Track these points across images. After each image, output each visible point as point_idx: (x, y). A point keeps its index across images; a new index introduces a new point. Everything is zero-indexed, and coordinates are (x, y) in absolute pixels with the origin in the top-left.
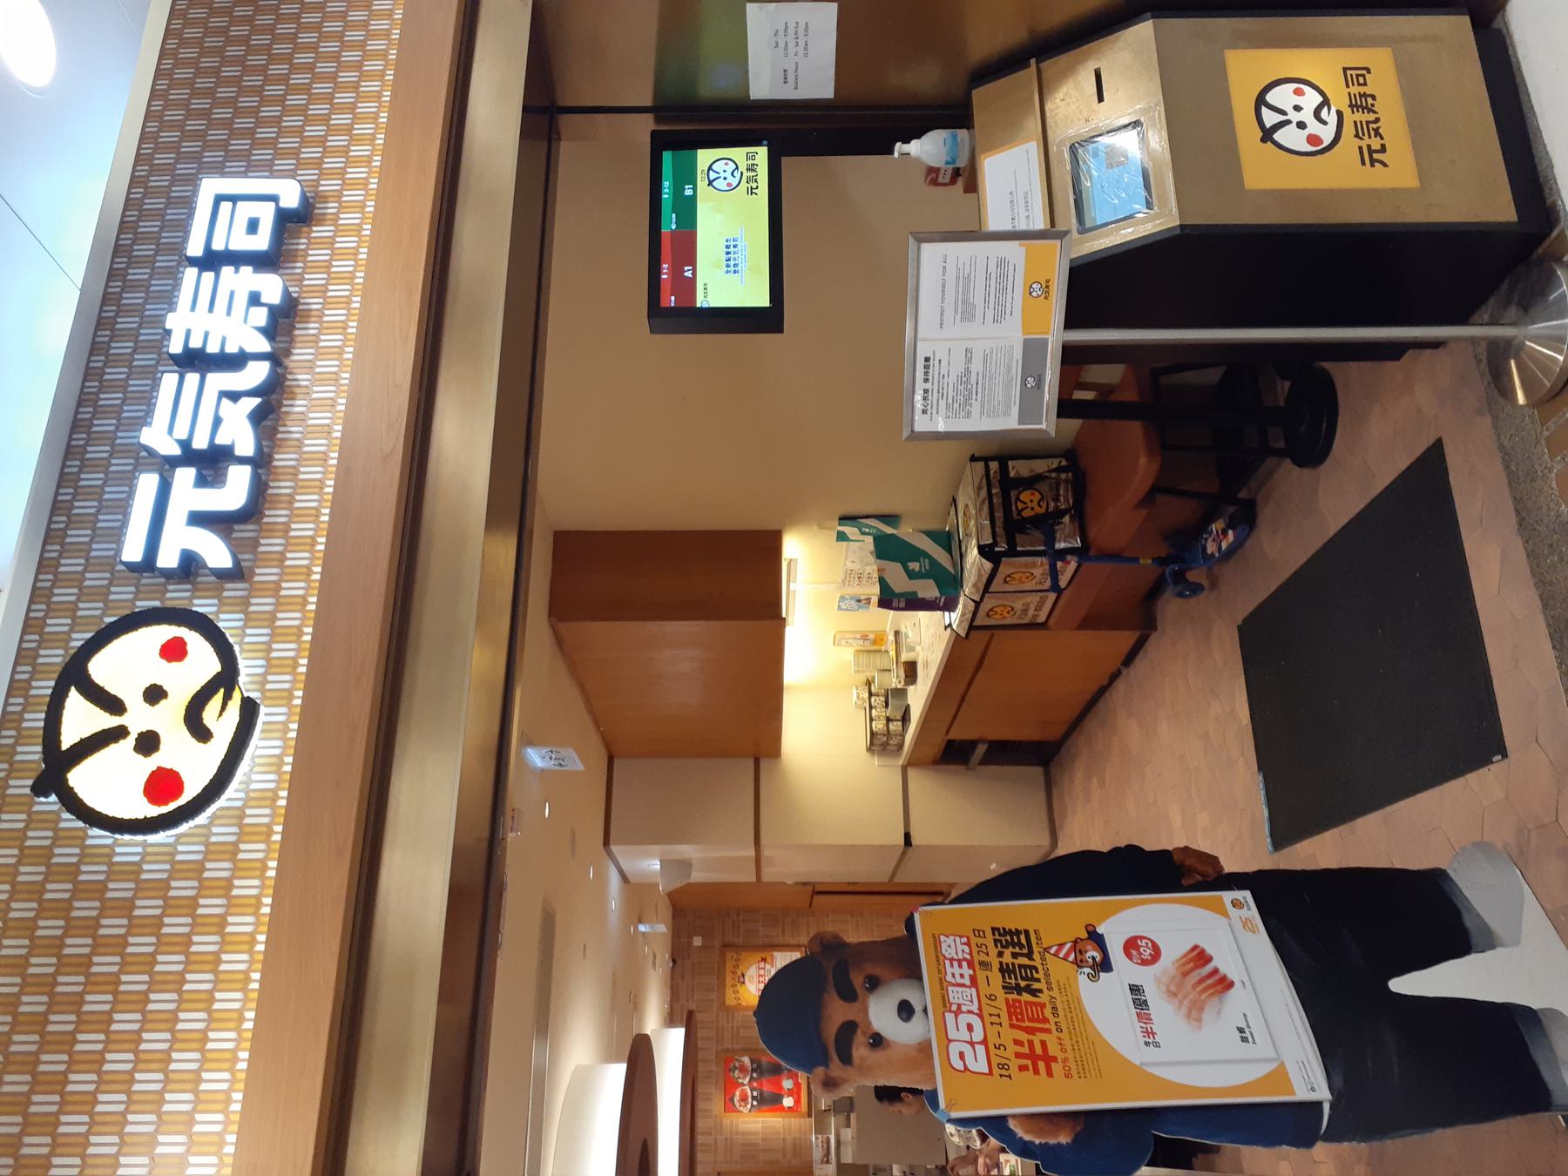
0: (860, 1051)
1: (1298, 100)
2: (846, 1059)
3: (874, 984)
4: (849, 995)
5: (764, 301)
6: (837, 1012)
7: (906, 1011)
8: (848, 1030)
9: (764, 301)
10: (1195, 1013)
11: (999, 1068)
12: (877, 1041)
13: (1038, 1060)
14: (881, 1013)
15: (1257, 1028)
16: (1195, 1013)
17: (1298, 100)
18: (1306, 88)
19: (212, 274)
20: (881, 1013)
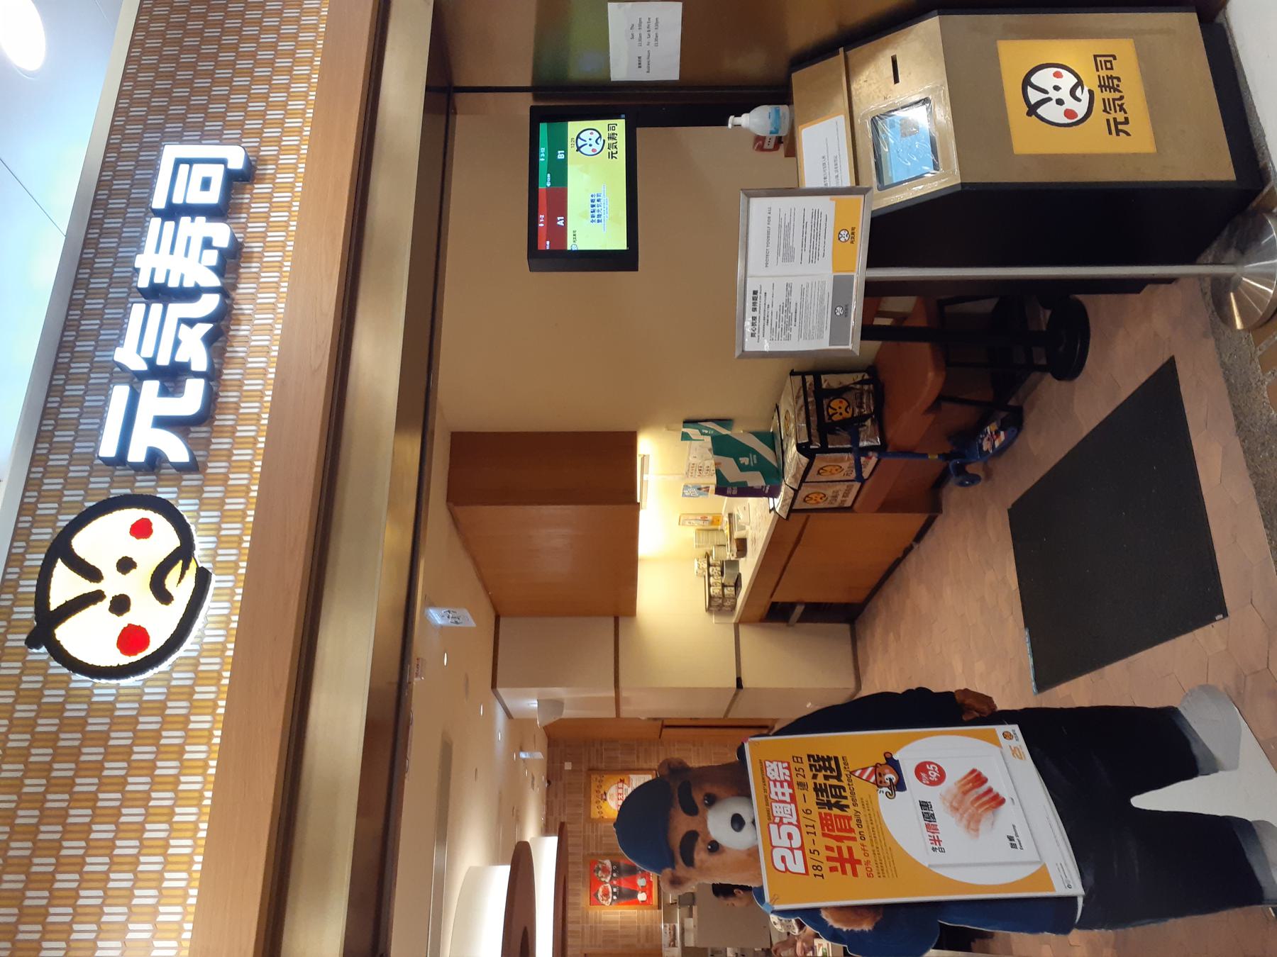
0: (700, 855)
1: (1057, 82)
2: (689, 862)
3: (712, 801)
4: (691, 810)
5: (623, 245)
6: (682, 824)
7: (738, 822)
8: (691, 838)
9: (623, 245)
10: (973, 824)
11: (813, 869)
12: (715, 847)
13: (846, 863)
14: (717, 824)
15: (1024, 836)
16: (973, 824)
17: (1057, 82)
18: (1064, 72)
19: (173, 223)
20: (717, 824)
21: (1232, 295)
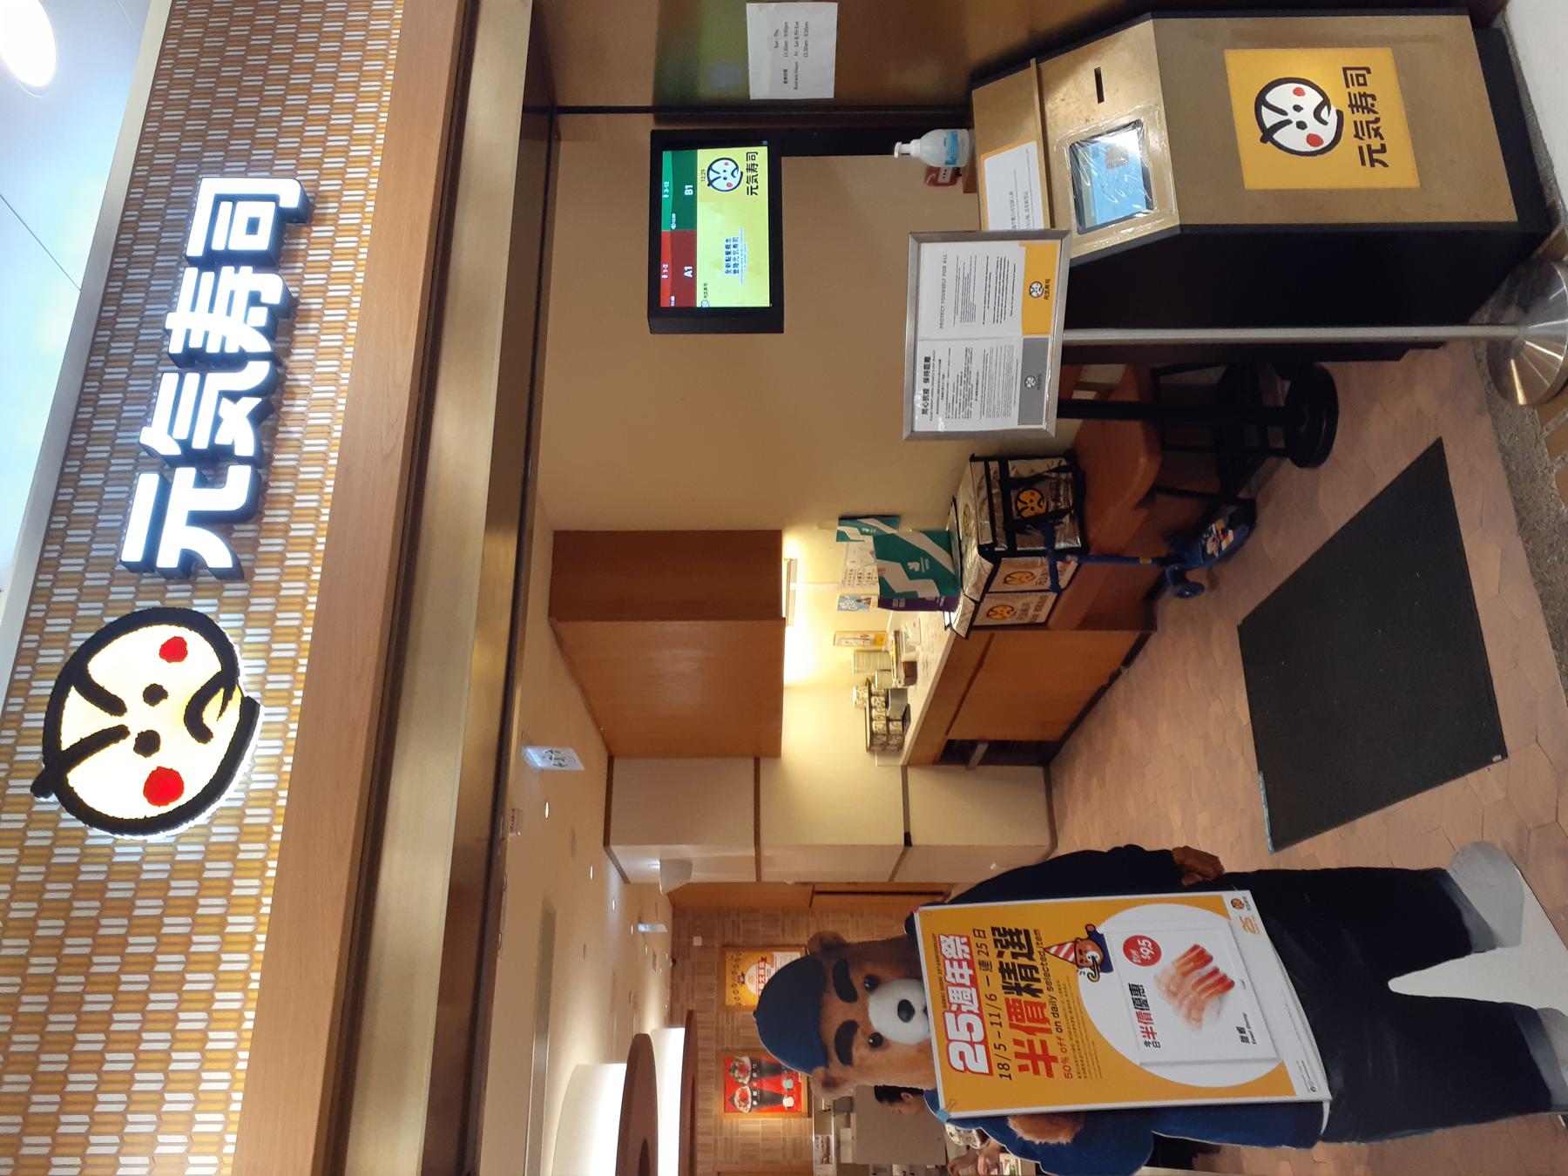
0: (860, 1051)
1: (1298, 100)
2: (846, 1059)
3: (874, 984)
4: (849, 995)
5: (764, 301)
6: (837, 1012)
7: (906, 1011)
8: (848, 1030)
9: (764, 301)
10: (1195, 1013)
11: (999, 1068)
12: (877, 1041)
13: (1038, 1060)
14: (881, 1013)
15: (1257, 1028)
16: (1195, 1013)
17: (1298, 100)
18: (1306, 88)
19: (212, 274)
20: (881, 1013)
21: (1513, 363)
